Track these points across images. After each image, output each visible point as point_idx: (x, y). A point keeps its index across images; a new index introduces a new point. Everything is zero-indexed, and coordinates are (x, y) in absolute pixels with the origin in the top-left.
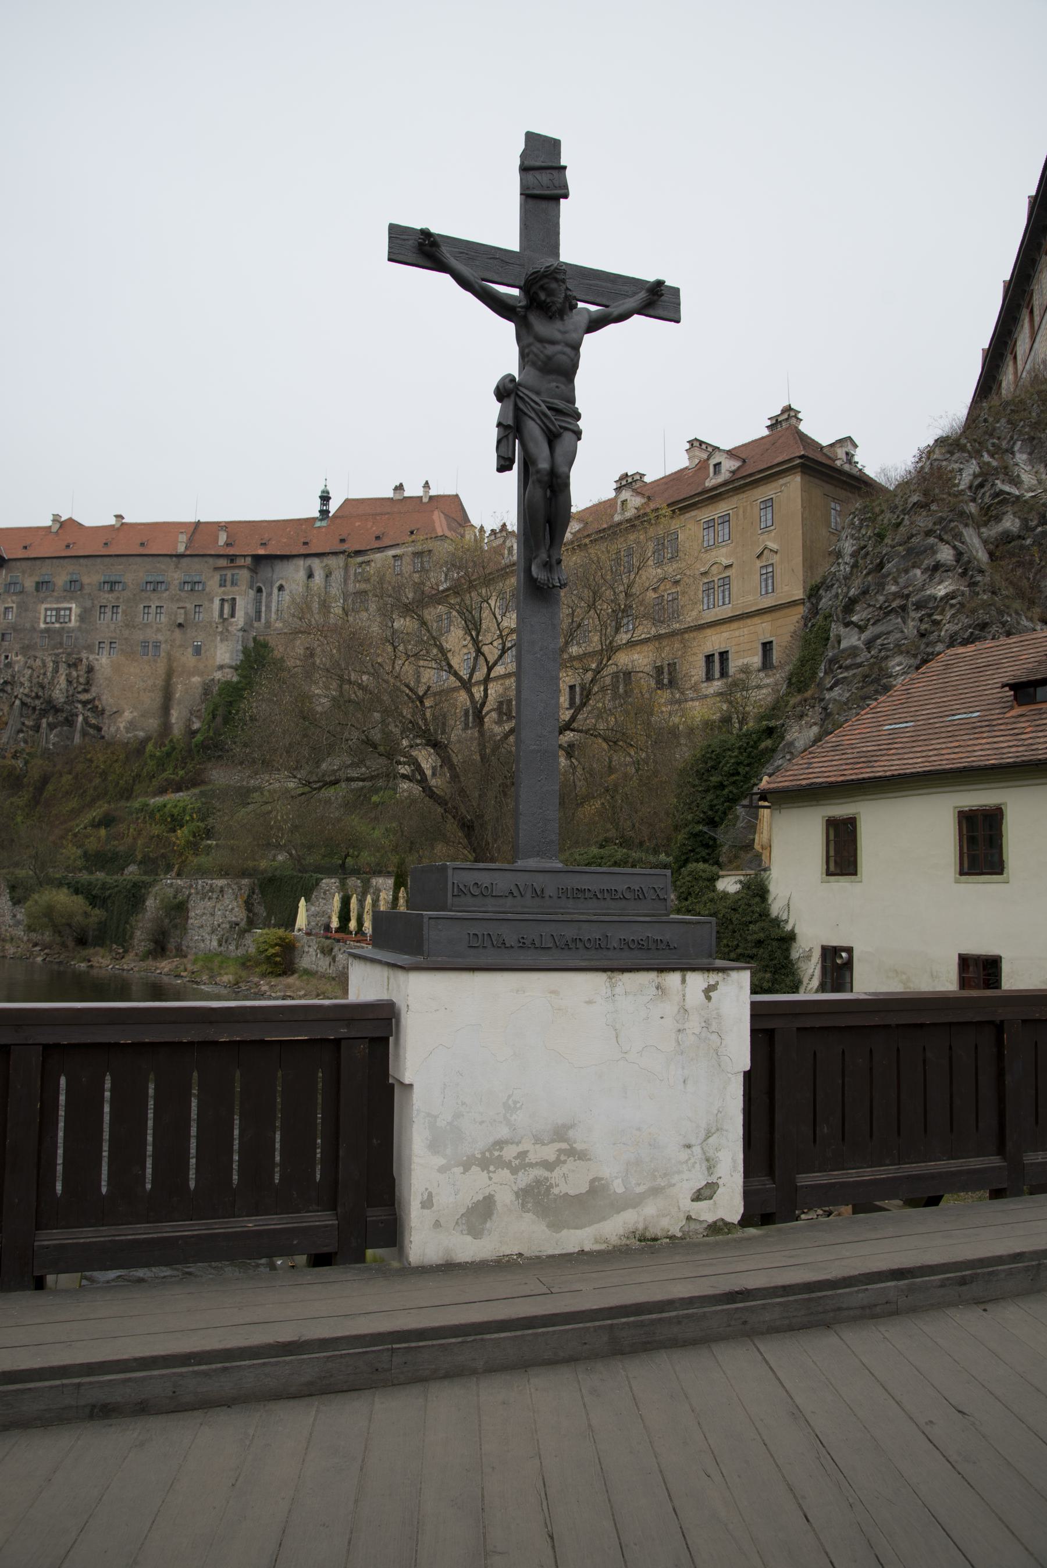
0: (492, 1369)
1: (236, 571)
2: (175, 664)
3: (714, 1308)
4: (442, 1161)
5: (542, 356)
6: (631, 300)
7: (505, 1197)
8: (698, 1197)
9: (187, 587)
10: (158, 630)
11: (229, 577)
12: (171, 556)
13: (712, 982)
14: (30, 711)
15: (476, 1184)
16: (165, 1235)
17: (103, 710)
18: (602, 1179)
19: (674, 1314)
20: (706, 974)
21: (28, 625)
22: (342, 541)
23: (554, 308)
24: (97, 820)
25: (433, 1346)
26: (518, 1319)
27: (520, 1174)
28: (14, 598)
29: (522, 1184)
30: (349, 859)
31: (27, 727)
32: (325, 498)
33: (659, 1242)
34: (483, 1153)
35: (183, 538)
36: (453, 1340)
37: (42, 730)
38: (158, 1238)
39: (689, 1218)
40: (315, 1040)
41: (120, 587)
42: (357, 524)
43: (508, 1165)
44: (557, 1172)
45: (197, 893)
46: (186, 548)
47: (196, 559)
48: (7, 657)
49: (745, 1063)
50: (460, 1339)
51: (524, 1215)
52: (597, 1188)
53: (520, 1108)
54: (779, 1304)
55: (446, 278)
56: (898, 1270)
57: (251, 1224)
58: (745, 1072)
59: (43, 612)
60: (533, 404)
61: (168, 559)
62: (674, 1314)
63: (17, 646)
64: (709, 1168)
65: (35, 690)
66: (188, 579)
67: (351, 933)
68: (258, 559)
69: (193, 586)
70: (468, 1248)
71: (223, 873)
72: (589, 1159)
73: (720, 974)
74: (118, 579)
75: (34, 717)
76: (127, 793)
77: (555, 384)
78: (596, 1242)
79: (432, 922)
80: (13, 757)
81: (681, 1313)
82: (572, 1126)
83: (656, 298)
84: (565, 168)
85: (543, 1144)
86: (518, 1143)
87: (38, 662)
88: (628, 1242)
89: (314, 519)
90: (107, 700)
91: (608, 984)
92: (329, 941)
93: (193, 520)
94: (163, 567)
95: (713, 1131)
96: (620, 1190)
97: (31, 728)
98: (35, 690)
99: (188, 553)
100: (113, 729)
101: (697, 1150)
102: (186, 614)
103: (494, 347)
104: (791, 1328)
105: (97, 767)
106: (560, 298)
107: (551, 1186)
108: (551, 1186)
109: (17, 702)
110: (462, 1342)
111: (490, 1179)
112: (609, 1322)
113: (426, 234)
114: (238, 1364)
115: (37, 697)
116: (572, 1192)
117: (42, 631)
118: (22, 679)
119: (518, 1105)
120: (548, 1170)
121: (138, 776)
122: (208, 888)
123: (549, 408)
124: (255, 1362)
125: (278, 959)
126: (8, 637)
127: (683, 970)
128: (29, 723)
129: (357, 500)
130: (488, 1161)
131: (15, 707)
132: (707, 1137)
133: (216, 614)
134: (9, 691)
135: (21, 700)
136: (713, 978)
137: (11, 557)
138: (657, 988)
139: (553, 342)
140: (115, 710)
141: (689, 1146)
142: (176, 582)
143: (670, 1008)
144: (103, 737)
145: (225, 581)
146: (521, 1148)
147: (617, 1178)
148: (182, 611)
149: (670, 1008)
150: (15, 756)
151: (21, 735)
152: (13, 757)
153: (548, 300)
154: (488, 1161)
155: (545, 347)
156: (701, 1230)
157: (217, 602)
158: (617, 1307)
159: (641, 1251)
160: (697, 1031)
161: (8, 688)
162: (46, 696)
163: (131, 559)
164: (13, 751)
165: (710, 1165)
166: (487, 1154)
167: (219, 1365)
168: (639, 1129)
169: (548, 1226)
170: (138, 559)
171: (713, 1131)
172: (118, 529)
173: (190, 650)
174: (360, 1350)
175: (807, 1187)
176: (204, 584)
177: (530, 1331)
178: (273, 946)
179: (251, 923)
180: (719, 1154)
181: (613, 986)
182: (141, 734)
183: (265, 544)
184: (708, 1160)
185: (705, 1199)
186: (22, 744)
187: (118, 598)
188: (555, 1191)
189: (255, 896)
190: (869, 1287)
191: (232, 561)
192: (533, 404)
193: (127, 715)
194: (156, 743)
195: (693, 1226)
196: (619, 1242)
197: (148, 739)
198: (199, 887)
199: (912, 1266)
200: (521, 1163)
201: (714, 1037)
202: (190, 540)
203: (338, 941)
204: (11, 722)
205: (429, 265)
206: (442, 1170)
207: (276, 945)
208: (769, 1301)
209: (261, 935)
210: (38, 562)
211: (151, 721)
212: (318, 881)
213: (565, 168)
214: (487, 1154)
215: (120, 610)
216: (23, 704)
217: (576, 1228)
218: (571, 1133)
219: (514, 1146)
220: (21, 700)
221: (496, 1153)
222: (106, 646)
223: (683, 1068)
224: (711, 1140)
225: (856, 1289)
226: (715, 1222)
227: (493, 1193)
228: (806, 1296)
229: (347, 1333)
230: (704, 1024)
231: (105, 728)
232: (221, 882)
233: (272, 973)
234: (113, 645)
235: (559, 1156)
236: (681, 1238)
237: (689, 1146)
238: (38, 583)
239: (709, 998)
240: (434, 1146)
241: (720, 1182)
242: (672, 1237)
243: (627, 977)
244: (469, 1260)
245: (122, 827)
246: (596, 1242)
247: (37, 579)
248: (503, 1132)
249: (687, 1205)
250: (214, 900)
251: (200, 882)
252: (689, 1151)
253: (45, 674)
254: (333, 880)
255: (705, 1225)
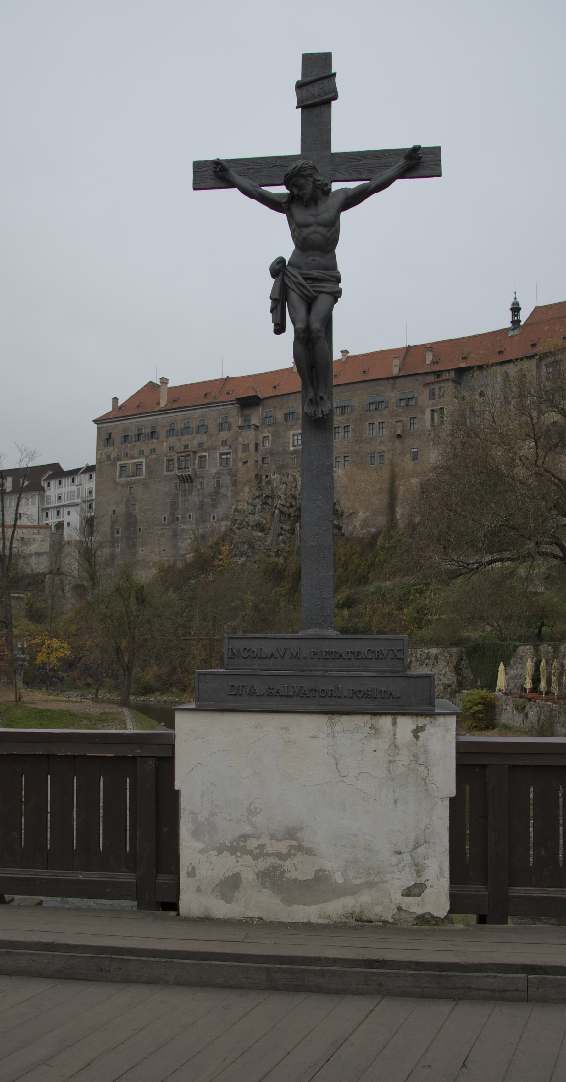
0: (180, 983)
1: (443, 384)
2: (397, 469)
3: (353, 969)
4: (201, 846)
5: (300, 238)
6: (391, 169)
7: (248, 876)
8: (408, 893)
9: (403, 403)
10: (382, 442)
11: (437, 392)
12: (387, 379)
13: (420, 725)
14: (287, 518)
15: (227, 864)
16: (29, 876)
17: (342, 513)
18: (325, 871)
19: (319, 968)
20: (415, 718)
21: (281, 450)
22: (534, 345)
23: (305, 199)
24: (341, 603)
25: (138, 960)
26: (199, 953)
27: (260, 860)
28: (269, 429)
29: (262, 868)
30: (544, 629)
31: (285, 530)
32: (516, 310)
33: (373, 924)
34: (232, 843)
35: (397, 362)
36: (152, 959)
37: (296, 533)
38: (24, 878)
39: (399, 909)
40: (119, 757)
41: (348, 410)
42: (546, 328)
43: (250, 853)
44: (288, 864)
45: (417, 660)
46: (400, 371)
47: (408, 379)
48: (267, 476)
49: (452, 791)
50: (157, 959)
51: (264, 890)
52: (321, 878)
53: (260, 812)
54: (412, 975)
55: (236, 191)
56: (530, 965)
57: (81, 875)
58: (451, 800)
59: (291, 437)
60: (293, 278)
61: (386, 382)
62: (319, 968)
63: (274, 467)
64: (417, 872)
65: (289, 500)
66: (403, 396)
67: (541, 693)
68: (461, 372)
69: (408, 402)
70: (220, 909)
71: (437, 644)
72: (315, 855)
73: (428, 718)
74: (346, 403)
75: (290, 522)
76: (364, 580)
77: (311, 258)
78: (321, 917)
79: (201, 677)
80: (275, 556)
81: (325, 968)
82: (301, 829)
83: (414, 162)
84: (335, 74)
85: (278, 840)
86: (258, 838)
87: (291, 478)
88: (347, 921)
89: (507, 330)
90: (345, 504)
91: (329, 724)
92: (522, 700)
93: (404, 346)
94: (382, 389)
95: (421, 842)
96: (340, 880)
97: (288, 531)
98: (289, 500)
99: (402, 374)
100: (350, 528)
101: (407, 857)
102: (403, 426)
103: (274, 236)
104: (422, 996)
105: (340, 559)
106: (309, 189)
107: (284, 872)
108: (284, 872)
109: (277, 512)
110: (166, 961)
111: (237, 861)
112: (267, 965)
113: (217, 163)
114: (17, 951)
115: (291, 506)
116: (301, 878)
117: (292, 453)
118: (279, 493)
119: (258, 810)
120: (281, 859)
121: (372, 564)
122: (425, 656)
123: (305, 279)
124: (26, 951)
125: (481, 715)
126: (267, 460)
127: (395, 714)
128: (287, 527)
129: (546, 306)
130: (236, 848)
131: (275, 516)
132: (416, 847)
133: (428, 423)
134: (271, 503)
135: (279, 509)
136: (421, 721)
137: (265, 396)
138: (371, 728)
139: (307, 226)
140: (351, 512)
141: (399, 853)
142: (394, 400)
143: (382, 744)
144: (343, 535)
145: (434, 394)
146: (260, 842)
147: (337, 871)
148: (400, 424)
149: (382, 744)
150: (277, 555)
151: (281, 538)
152: (275, 556)
153: (300, 194)
154: (236, 848)
155: (301, 231)
156: (411, 920)
157: (428, 413)
158: (273, 956)
159: (355, 929)
160: (406, 763)
161: (270, 501)
162: (298, 505)
163: (356, 385)
164: (275, 550)
165: (419, 869)
166: (235, 844)
167: (6, 950)
168: (356, 836)
169: (281, 901)
170: (362, 385)
171: (421, 842)
172: (345, 362)
173: (408, 456)
174: (91, 955)
175: (518, 897)
176: (417, 399)
177: (206, 962)
178: (476, 705)
179: (461, 685)
180: (427, 861)
181: (333, 726)
182: (373, 530)
183: (465, 358)
184: (416, 865)
185: (414, 896)
186: (282, 545)
187: (348, 419)
188: (288, 875)
189: (463, 662)
190: (498, 975)
191: (438, 376)
192: (293, 278)
193: (361, 515)
194: (385, 537)
195: (403, 915)
196: (339, 920)
197: (379, 533)
198: (418, 655)
199: (545, 964)
200: (260, 853)
201: (422, 768)
202: (403, 363)
203: (530, 700)
204: (273, 528)
205: (223, 186)
206: (202, 851)
207: (479, 703)
208: (403, 972)
209: (467, 695)
210: (285, 398)
211: (380, 518)
212: (515, 649)
213: (335, 74)
214: (235, 844)
215: (350, 429)
216: (281, 512)
217: (304, 904)
218: (299, 834)
219: (255, 840)
220: (279, 509)
221: (242, 844)
222: (341, 459)
223: (394, 791)
224: (419, 850)
225: (485, 974)
226: (423, 915)
227: (239, 872)
228: (437, 973)
229: (84, 943)
230: (412, 758)
231: (344, 527)
232: (434, 651)
233: (476, 727)
234: (347, 459)
235: (290, 851)
236: (393, 923)
237: (399, 853)
238: (286, 415)
239: (417, 737)
240: (196, 834)
241: (428, 884)
242: (385, 922)
243: (344, 719)
244: (221, 917)
245: (361, 607)
246: (321, 917)
247: (285, 412)
248: (247, 829)
249: (397, 897)
250: (431, 666)
251: (419, 651)
252: (400, 857)
253: (296, 487)
254: (528, 647)
255: (415, 916)
